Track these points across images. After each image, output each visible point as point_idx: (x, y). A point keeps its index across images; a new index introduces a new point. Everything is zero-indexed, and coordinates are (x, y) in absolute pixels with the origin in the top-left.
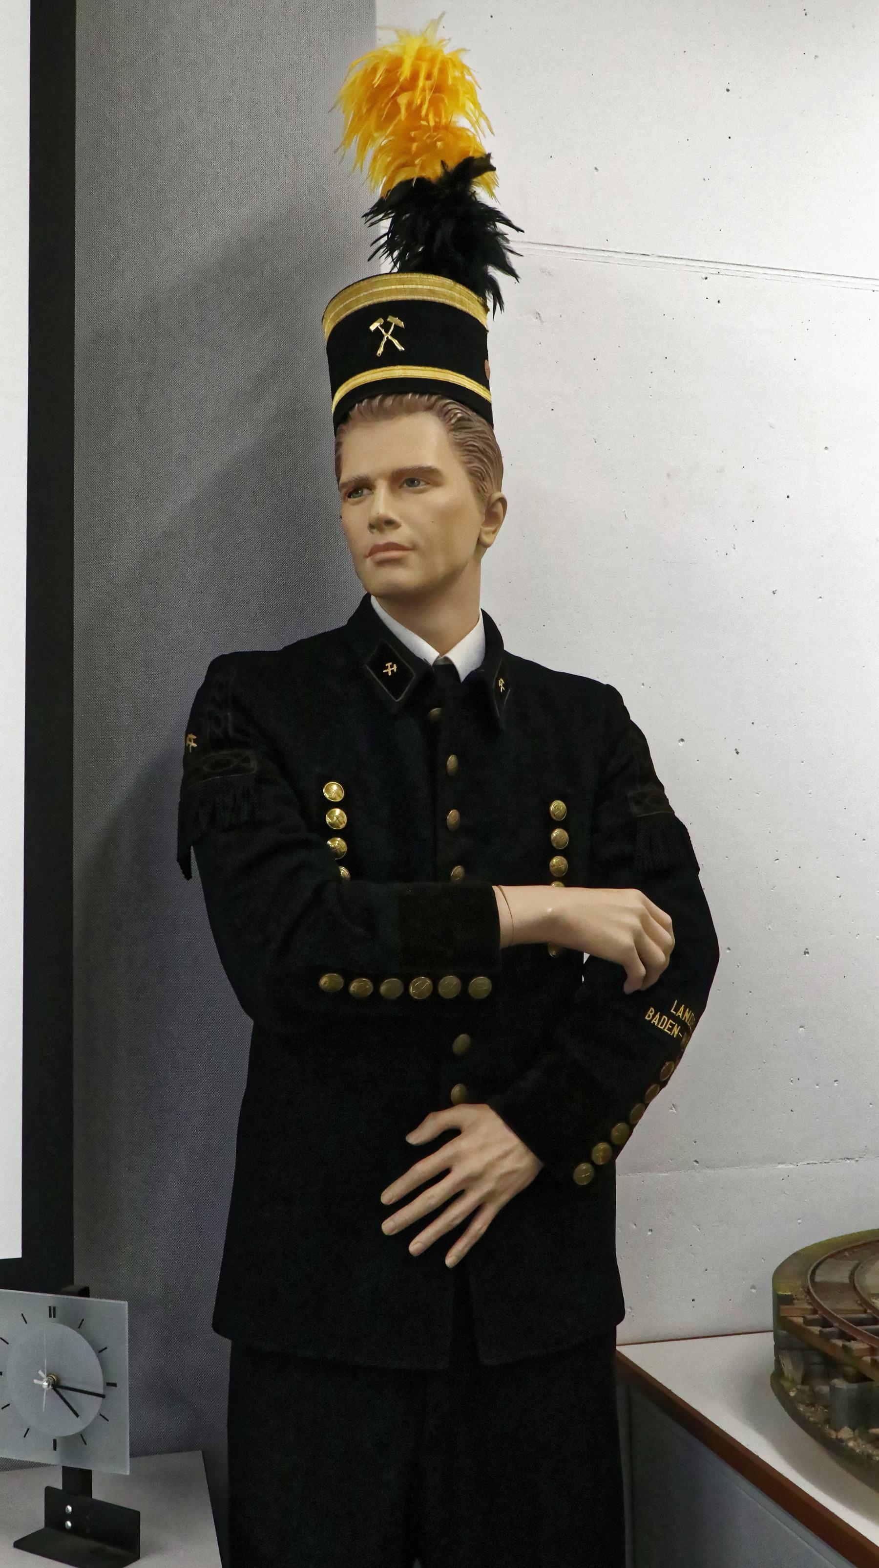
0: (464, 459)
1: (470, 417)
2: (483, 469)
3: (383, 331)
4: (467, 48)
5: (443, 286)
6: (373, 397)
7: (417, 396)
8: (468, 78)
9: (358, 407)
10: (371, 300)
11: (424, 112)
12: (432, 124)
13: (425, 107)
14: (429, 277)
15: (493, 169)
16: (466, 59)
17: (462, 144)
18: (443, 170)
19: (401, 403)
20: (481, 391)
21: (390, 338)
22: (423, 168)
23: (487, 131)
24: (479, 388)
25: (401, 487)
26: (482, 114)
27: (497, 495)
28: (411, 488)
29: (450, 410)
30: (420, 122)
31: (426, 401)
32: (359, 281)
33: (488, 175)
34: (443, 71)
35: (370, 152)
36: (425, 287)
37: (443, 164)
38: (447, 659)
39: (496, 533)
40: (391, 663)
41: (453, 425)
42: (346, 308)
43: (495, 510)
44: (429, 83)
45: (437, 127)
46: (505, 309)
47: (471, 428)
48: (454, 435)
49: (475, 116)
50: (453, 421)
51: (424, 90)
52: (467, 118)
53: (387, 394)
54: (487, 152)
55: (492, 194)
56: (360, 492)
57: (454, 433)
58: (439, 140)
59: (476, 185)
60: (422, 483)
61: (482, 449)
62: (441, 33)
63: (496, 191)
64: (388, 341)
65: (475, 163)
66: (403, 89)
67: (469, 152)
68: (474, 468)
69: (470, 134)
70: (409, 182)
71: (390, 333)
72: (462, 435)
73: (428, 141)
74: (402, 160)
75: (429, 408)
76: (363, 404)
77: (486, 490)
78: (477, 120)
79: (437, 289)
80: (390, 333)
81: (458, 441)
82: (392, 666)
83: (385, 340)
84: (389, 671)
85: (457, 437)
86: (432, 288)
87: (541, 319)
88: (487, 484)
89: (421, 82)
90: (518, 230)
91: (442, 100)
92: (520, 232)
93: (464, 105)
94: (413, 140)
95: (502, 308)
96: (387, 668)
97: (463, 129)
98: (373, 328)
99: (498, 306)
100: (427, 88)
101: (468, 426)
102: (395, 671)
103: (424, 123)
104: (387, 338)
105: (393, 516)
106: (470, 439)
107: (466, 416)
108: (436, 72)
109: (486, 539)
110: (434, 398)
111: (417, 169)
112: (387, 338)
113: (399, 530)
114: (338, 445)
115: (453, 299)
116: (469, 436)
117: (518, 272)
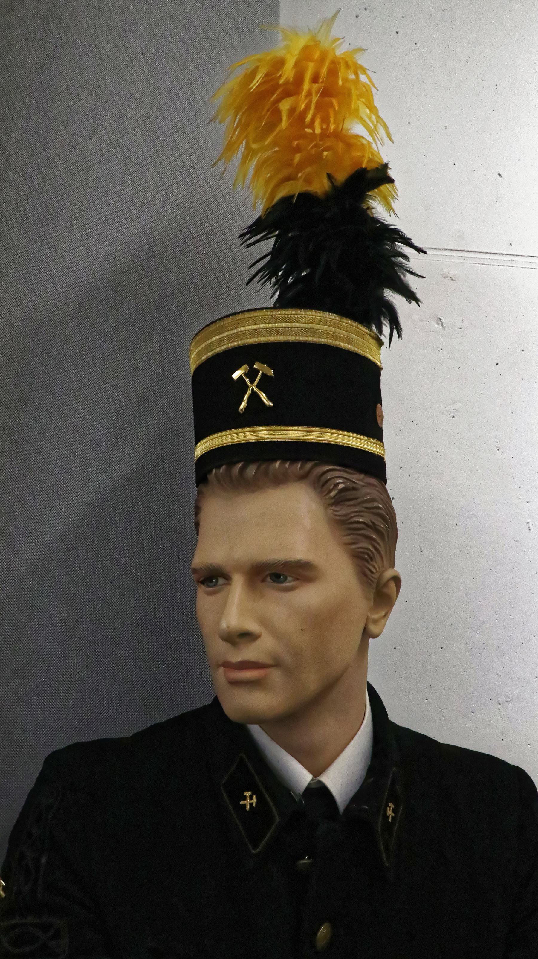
0: (348, 539)
1: (354, 485)
2: (371, 548)
3: (247, 381)
4: (365, 48)
5: (325, 322)
6: (232, 464)
7: (287, 465)
8: (363, 78)
9: (215, 474)
10: (235, 341)
11: (308, 118)
12: (318, 131)
13: (311, 112)
14: (308, 313)
15: (391, 181)
16: (361, 60)
17: (368, 155)
18: (330, 184)
19: (266, 473)
20: (371, 446)
21: (255, 389)
22: (308, 181)
23: (386, 139)
24: (369, 443)
25: (263, 581)
26: (378, 118)
27: (389, 574)
28: (275, 584)
29: (328, 481)
30: (305, 130)
31: (298, 470)
32: (222, 318)
33: (385, 188)
34: (333, 72)
35: (252, 166)
36: (302, 325)
37: (330, 177)
38: (320, 782)
39: (386, 617)
40: (250, 793)
41: (332, 498)
42: (208, 348)
43: (385, 590)
44: (316, 86)
45: (325, 135)
46: (403, 336)
47: (356, 499)
48: (334, 511)
49: (372, 122)
50: (333, 494)
51: (309, 94)
52: (364, 126)
53: (248, 462)
54: (385, 161)
55: (390, 208)
56: (214, 581)
57: (333, 508)
58: (327, 149)
59: (372, 199)
60: (289, 579)
61: (370, 522)
62: (336, 31)
63: (395, 205)
64: (253, 393)
65: (369, 175)
66: (287, 94)
67: (361, 163)
68: (360, 550)
69: (364, 142)
70: (290, 197)
71: (255, 384)
72: (343, 510)
73: (313, 151)
74: (285, 172)
75: (302, 477)
76: (221, 471)
77: (374, 571)
78: (375, 127)
79: (317, 326)
80: (255, 384)
81: (337, 518)
82: (251, 798)
83: (249, 391)
84: (247, 802)
85: (337, 513)
86: (311, 326)
87: (442, 325)
88: (377, 564)
89: (306, 86)
90: (419, 250)
91: (331, 105)
92: (421, 253)
93: (357, 110)
94: (298, 149)
95: (399, 335)
96: (245, 798)
97: (357, 137)
98: (236, 375)
99: (395, 332)
100: (314, 92)
101: (351, 497)
102: (254, 805)
103: (308, 130)
104: (253, 390)
105: (252, 626)
106: (355, 514)
107: (350, 485)
108: (324, 71)
109: (373, 628)
110: (309, 465)
111: (301, 182)
112: (253, 390)
113: (258, 642)
114: (198, 510)
115: (337, 337)
116: (353, 510)
117: (418, 296)
